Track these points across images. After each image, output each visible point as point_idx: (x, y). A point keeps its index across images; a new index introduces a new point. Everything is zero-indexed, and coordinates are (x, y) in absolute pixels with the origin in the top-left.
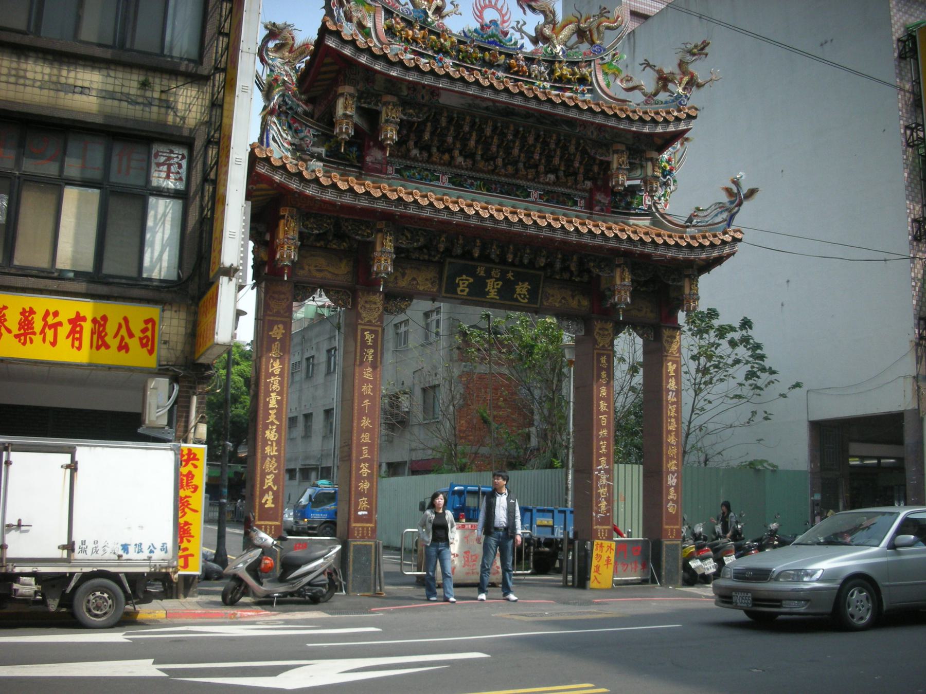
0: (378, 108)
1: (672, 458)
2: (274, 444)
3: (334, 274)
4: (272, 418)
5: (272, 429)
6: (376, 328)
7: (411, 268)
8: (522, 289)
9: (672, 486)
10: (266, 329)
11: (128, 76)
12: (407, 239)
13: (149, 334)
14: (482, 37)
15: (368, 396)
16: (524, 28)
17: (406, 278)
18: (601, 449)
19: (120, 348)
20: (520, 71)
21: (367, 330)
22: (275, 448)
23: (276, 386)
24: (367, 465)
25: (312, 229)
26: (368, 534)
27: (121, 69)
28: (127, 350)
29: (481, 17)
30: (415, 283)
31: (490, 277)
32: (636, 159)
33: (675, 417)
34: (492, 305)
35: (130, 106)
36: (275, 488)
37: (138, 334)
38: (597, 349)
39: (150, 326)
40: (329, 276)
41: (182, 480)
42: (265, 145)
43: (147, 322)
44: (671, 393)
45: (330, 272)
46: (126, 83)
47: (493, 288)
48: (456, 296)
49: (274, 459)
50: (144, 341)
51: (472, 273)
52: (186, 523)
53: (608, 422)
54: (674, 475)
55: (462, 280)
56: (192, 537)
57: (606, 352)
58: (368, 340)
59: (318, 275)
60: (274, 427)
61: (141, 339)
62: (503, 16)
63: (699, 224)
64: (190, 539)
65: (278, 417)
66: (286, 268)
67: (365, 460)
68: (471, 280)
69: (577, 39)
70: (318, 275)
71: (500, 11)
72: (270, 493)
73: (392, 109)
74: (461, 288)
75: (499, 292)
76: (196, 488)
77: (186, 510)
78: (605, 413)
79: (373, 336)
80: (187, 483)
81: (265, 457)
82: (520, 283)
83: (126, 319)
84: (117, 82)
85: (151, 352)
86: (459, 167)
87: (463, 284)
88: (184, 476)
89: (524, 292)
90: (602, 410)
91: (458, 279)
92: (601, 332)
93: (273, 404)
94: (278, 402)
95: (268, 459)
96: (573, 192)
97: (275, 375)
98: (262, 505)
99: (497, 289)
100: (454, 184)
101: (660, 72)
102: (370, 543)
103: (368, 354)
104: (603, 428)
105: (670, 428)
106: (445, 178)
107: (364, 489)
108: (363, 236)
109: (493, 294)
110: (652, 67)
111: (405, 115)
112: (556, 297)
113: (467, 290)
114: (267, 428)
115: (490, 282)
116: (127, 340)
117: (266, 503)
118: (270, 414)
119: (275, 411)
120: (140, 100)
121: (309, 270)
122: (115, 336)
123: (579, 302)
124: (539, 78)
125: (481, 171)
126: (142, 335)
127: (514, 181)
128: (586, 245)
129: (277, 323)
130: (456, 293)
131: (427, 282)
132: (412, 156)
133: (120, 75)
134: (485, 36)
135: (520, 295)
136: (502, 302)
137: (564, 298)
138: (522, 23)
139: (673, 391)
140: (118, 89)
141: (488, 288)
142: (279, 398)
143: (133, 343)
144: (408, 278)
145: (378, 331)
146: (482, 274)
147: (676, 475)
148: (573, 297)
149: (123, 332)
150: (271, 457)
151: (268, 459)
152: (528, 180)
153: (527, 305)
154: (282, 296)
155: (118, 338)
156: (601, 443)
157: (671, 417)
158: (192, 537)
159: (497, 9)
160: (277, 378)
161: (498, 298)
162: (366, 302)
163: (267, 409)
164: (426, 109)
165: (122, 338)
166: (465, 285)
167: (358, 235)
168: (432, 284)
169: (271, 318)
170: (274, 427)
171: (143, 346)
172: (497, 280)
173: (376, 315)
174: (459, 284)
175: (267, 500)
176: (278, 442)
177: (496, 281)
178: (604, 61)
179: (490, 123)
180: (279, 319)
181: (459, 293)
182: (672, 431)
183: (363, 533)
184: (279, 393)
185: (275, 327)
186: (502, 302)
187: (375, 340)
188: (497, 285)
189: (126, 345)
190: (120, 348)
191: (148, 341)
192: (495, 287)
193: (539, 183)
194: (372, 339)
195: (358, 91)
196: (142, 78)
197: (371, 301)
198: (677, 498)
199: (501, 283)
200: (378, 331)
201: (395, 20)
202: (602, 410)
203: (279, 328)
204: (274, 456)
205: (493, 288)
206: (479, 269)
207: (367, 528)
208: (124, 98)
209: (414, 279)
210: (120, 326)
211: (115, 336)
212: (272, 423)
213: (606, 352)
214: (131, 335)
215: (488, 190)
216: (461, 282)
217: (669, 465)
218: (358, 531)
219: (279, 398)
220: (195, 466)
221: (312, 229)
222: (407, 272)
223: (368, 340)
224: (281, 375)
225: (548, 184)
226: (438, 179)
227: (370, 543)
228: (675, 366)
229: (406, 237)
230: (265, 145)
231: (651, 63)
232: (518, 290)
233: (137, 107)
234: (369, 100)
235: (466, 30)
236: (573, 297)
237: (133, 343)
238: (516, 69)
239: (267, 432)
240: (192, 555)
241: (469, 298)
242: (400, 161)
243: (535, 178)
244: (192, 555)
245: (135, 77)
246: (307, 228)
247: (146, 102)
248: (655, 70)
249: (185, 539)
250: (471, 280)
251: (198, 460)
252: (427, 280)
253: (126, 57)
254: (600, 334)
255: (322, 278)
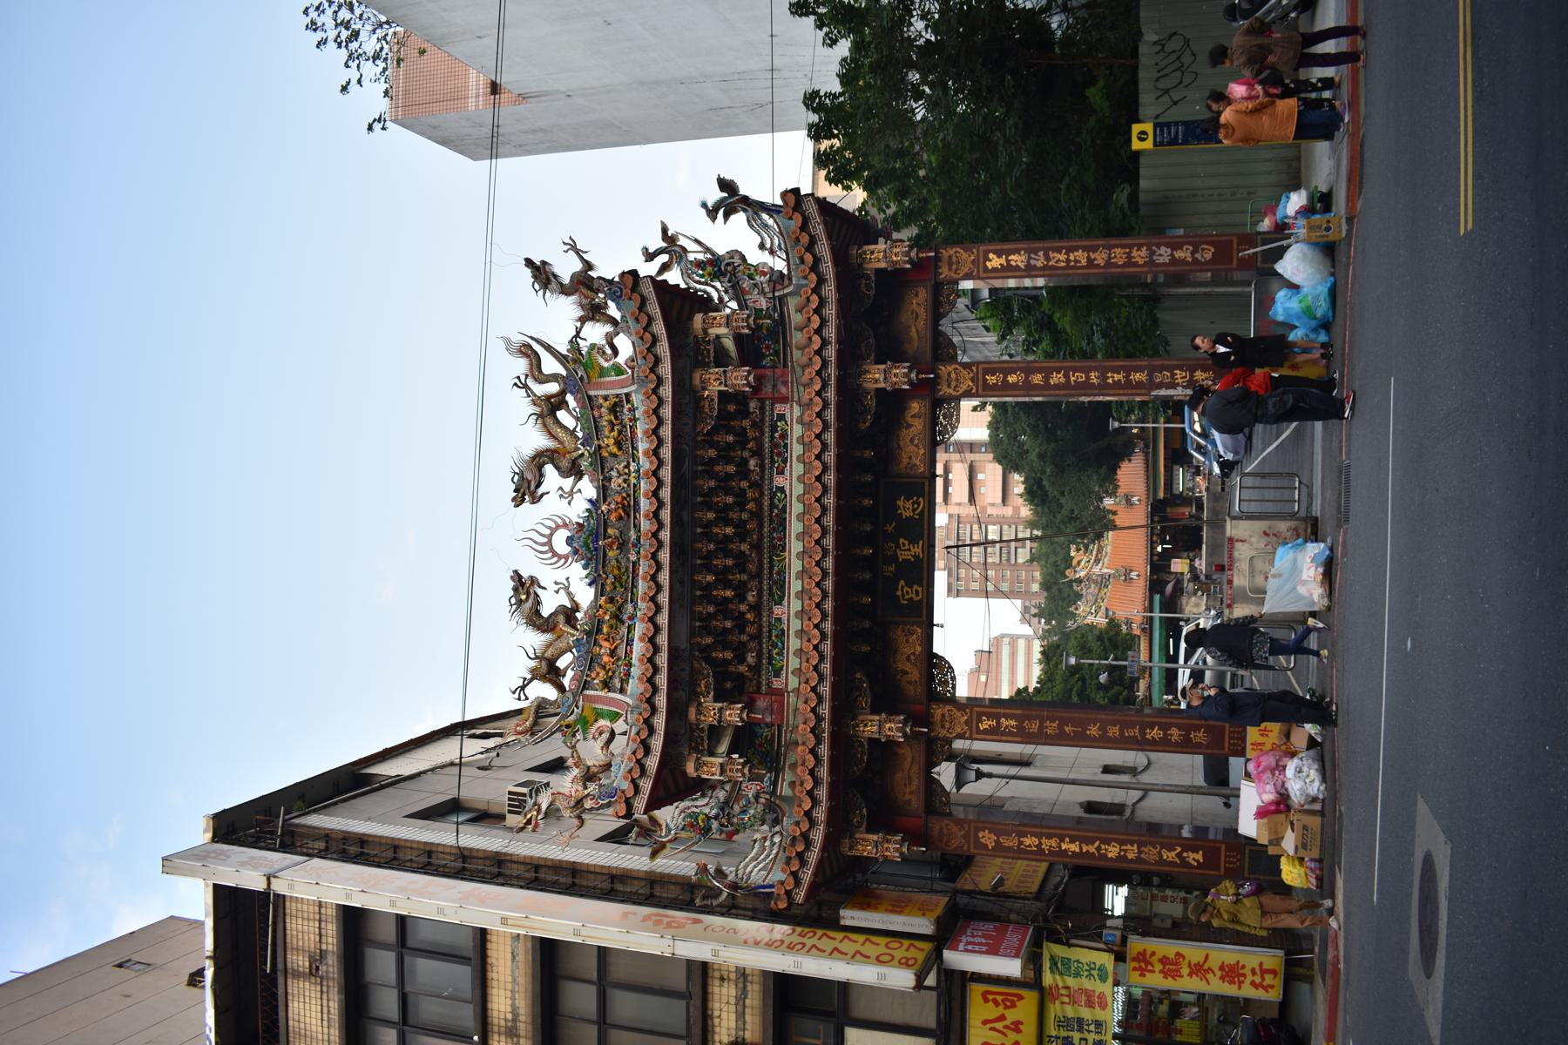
1: (1129, 256)
2: (1123, 847)
3: (912, 763)
4: (1092, 849)
5: (1106, 850)
9: (1172, 255)
10: (985, 852)
11: (716, 997)
12: (860, 695)
13: (999, 998)
15: (1060, 727)
18: (1120, 380)
19: (1018, 1031)
22: (1129, 847)
23: (1053, 842)
24: (1148, 731)
26: (1238, 732)
27: (710, 1004)
28: (1019, 1023)
30: (912, 657)
32: (708, 351)
33: (1067, 254)
35: (749, 996)
36: (1179, 849)
37: (1000, 1010)
39: (990, 997)
40: (915, 770)
41: (1169, 970)
43: (986, 1001)
44: (1032, 262)
46: (725, 999)
47: (909, 550)
48: (925, 601)
49: (1143, 849)
50: (1008, 1004)
52: (1222, 968)
53: (1080, 370)
54: (1155, 252)
55: (903, 594)
56: (1238, 962)
57: (980, 376)
59: (915, 782)
60: (1103, 847)
61: (1006, 1007)
62: (558, 527)
64: (1241, 964)
65: (1090, 841)
67: (1143, 734)
69: (563, 411)
70: (915, 782)
72: (1185, 854)
74: (914, 596)
75: (913, 541)
76: (1179, 955)
77: (1206, 967)
78: (1066, 376)
80: (1173, 964)
81: (1139, 860)
83: (985, 1022)
84: (725, 1008)
85: (1020, 997)
86: (760, 595)
87: (907, 592)
88: (1164, 967)
89: (909, 504)
90: (1063, 380)
91: (902, 602)
92: (953, 384)
93: (1074, 847)
94: (1072, 841)
95: (1142, 856)
97: (1041, 844)
98: (1200, 866)
100: (782, 598)
102: (1247, 851)
103: (1007, 726)
104: (1088, 378)
105: (1084, 262)
106: (777, 610)
107: (1180, 735)
108: (862, 753)
109: (917, 550)
112: (911, 452)
113: (915, 587)
114: (1105, 855)
115: (903, 555)
116: (1007, 1022)
117: (1198, 861)
118: (1088, 851)
119: (1084, 846)
120: (741, 985)
122: (1006, 1035)
124: (626, 477)
126: (1002, 1007)
128: (839, 457)
129: (977, 838)
130: (921, 601)
132: (755, 599)
133: (716, 1005)
134: (589, 556)
135: (914, 510)
136: (926, 536)
138: (560, 492)
139: (1030, 258)
140: (733, 1008)
142: (1067, 839)
143: (1012, 1015)
144: (908, 667)
146: (892, 568)
147: (1154, 248)
148: (909, 426)
149: (999, 1025)
150: (1140, 852)
151: (1142, 856)
152: (762, 494)
154: (945, 831)
155: (1005, 1031)
156: (1110, 381)
157: (1068, 261)
158: (1238, 962)
159: (551, 535)
160: (1043, 840)
162: (943, 727)
163: (1080, 854)
164: (696, 665)
165: (1005, 1027)
166: (910, 590)
168: (912, 634)
169: (972, 846)
170: (1103, 847)
171: (1013, 1005)
172: (898, 546)
174: (908, 600)
175: (1194, 859)
176: (1121, 843)
178: (585, 377)
179: (699, 514)
182: (1088, 258)
183: (1238, 739)
184: (1062, 840)
185: (982, 840)
187: (990, 716)
188: (904, 545)
189: (1013, 1023)
190: (1018, 1031)
191: (1009, 1001)
193: (762, 478)
195: (690, 754)
196: (717, 983)
197: (942, 721)
198: (1189, 243)
199: (902, 540)
202: (1063, 380)
204: (1139, 848)
205: (909, 550)
206: (888, 574)
207: (1230, 732)
208: (741, 1002)
209: (908, 658)
210: (992, 1029)
211: (1006, 1035)
212: (1099, 849)
213: (980, 376)
214: (1002, 1018)
215: (784, 550)
216: (907, 597)
217: (1141, 261)
218: (1234, 744)
219: (1067, 839)
220: (1153, 954)
221: (862, 816)
222: (900, 666)
224: (1039, 836)
225: (762, 466)
226: (779, 620)
227: (1247, 851)
228: (991, 256)
229: (858, 696)
231: (574, 333)
232: (909, 514)
233: (749, 988)
236: (909, 426)
237: (1012, 1015)
238: (621, 511)
239: (1110, 855)
240: (1261, 964)
244: (1261, 964)
245: (716, 990)
247: (742, 979)
248: (582, 327)
249: (1241, 972)
251: (1145, 950)
252: (907, 641)
253: (696, 990)
255: (918, 778)
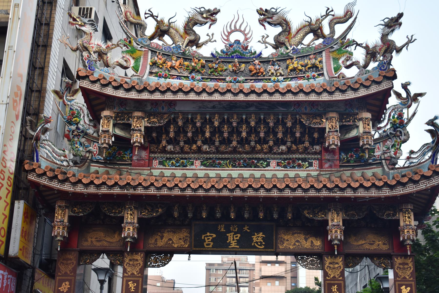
0: (129, 122)
6: (138, 279)
7: (168, 232)
8: (258, 238)
10: (57, 285)
14: (227, 54)
16: (268, 40)
17: (164, 239)
20: (258, 73)
21: (130, 281)
25: (78, 213)
29: (228, 40)
30: (171, 242)
31: (230, 232)
32: (349, 121)
34: (236, 253)
38: (399, 281)
40: (105, 244)
42: (35, 162)
45: (107, 241)
47: (233, 240)
51: (214, 230)
57: (336, 282)
58: (131, 288)
63: (412, 165)
66: (129, 243)
68: (214, 236)
70: (98, 244)
71: (243, 32)
73: (137, 121)
75: (238, 242)
79: (135, 284)
82: (256, 234)
89: (260, 239)
91: (203, 236)
92: (331, 266)
96: (306, 156)
99: (236, 240)
100: (205, 165)
101: (367, 47)
106: (198, 163)
109: (234, 244)
110: (407, 44)
111: (150, 123)
113: (212, 243)
115: (230, 236)
121: (92, 242)
123: (312, 242)
125: (223, 153)
127: (257, 156)
130: (204, 247)
131: (181, 241)
134: (229, 53)
135: (257, 243)
136: (242, 250)
137: (298, 241)
141: (229, 240)
144: (165, 239)
145: (412, 284)
146: (223, 230)
148: (306, 240)
152: (266, 153)
153: (264, 250)
154: (69, 262)
159: (241, 31)
161: (238, 247)
162: (130, 260)
164: (166, 116)
166: (210, 240)
167: (112, 213)
172: (236, 233)
173: (138, 269)
177: (235, 234)
180: (66, 278)
181: (206, 246)
185: (64, 284)
186: (242, 250)
188: (237, 237)
192: (235, 239)
193: (275, 153)
194: (134, 287)
195: (115, 112)
197: (134, 259)
199: (239, 235)
200: (412, 284)
201: (157, 57)
203: (66, 284)
205: (233, 240)
209: (170, 239)
213: (336, 282)
215: (233, 166)
221: (78, 213)
223: (131, 288)
225: (282, 153)
226: (192, 164)
230: (35, 162)
231: (359, 43)
232: (255, 239)
234: (122, 118)
235: (214, 53)
236: (306, 240)
241: (214, 249)
242: (162, 155)
243: (305, 151)
246: (74, 213)
248: (363, 47)
250: (214, 236)
252: (180, 239)
254: (330, 267)
